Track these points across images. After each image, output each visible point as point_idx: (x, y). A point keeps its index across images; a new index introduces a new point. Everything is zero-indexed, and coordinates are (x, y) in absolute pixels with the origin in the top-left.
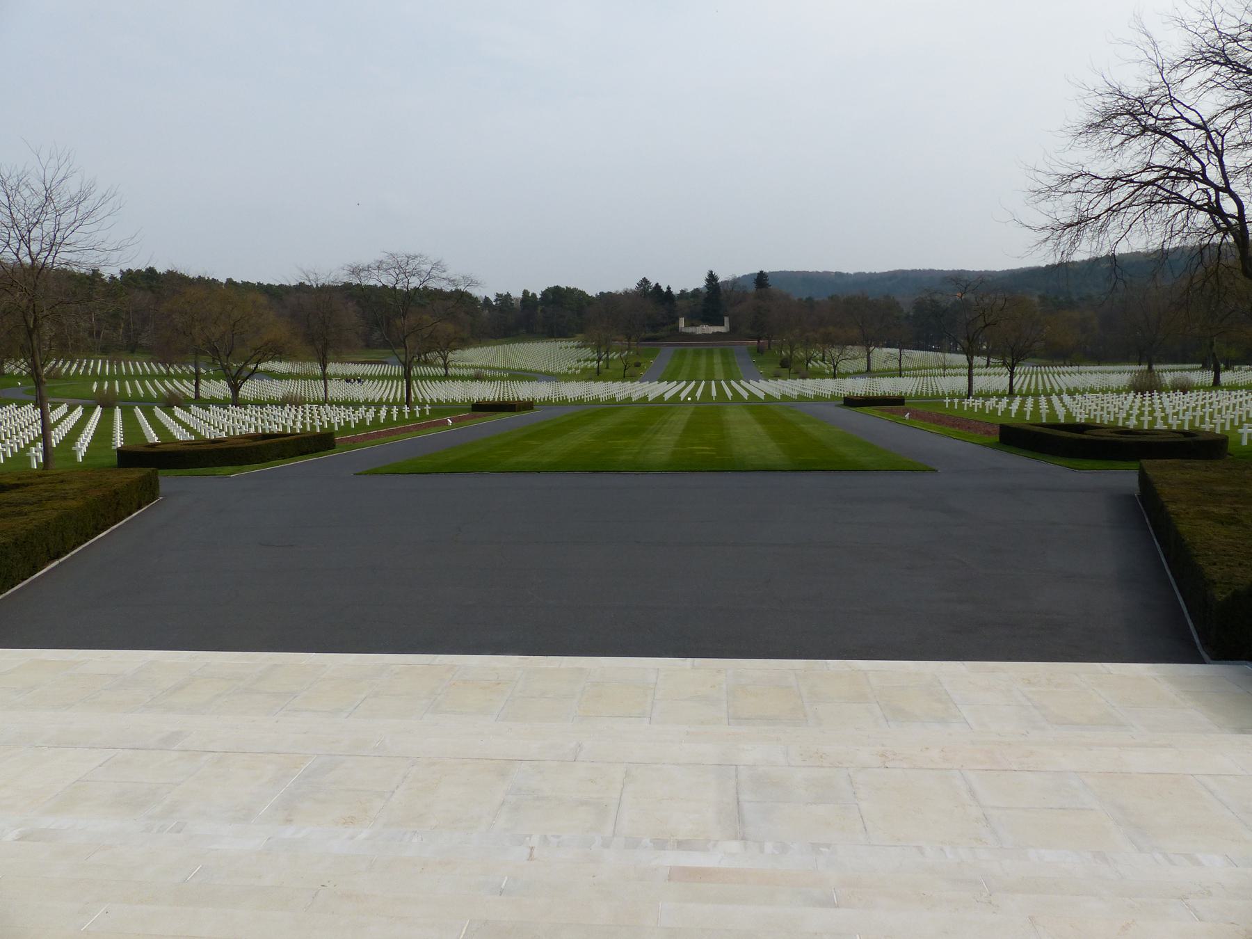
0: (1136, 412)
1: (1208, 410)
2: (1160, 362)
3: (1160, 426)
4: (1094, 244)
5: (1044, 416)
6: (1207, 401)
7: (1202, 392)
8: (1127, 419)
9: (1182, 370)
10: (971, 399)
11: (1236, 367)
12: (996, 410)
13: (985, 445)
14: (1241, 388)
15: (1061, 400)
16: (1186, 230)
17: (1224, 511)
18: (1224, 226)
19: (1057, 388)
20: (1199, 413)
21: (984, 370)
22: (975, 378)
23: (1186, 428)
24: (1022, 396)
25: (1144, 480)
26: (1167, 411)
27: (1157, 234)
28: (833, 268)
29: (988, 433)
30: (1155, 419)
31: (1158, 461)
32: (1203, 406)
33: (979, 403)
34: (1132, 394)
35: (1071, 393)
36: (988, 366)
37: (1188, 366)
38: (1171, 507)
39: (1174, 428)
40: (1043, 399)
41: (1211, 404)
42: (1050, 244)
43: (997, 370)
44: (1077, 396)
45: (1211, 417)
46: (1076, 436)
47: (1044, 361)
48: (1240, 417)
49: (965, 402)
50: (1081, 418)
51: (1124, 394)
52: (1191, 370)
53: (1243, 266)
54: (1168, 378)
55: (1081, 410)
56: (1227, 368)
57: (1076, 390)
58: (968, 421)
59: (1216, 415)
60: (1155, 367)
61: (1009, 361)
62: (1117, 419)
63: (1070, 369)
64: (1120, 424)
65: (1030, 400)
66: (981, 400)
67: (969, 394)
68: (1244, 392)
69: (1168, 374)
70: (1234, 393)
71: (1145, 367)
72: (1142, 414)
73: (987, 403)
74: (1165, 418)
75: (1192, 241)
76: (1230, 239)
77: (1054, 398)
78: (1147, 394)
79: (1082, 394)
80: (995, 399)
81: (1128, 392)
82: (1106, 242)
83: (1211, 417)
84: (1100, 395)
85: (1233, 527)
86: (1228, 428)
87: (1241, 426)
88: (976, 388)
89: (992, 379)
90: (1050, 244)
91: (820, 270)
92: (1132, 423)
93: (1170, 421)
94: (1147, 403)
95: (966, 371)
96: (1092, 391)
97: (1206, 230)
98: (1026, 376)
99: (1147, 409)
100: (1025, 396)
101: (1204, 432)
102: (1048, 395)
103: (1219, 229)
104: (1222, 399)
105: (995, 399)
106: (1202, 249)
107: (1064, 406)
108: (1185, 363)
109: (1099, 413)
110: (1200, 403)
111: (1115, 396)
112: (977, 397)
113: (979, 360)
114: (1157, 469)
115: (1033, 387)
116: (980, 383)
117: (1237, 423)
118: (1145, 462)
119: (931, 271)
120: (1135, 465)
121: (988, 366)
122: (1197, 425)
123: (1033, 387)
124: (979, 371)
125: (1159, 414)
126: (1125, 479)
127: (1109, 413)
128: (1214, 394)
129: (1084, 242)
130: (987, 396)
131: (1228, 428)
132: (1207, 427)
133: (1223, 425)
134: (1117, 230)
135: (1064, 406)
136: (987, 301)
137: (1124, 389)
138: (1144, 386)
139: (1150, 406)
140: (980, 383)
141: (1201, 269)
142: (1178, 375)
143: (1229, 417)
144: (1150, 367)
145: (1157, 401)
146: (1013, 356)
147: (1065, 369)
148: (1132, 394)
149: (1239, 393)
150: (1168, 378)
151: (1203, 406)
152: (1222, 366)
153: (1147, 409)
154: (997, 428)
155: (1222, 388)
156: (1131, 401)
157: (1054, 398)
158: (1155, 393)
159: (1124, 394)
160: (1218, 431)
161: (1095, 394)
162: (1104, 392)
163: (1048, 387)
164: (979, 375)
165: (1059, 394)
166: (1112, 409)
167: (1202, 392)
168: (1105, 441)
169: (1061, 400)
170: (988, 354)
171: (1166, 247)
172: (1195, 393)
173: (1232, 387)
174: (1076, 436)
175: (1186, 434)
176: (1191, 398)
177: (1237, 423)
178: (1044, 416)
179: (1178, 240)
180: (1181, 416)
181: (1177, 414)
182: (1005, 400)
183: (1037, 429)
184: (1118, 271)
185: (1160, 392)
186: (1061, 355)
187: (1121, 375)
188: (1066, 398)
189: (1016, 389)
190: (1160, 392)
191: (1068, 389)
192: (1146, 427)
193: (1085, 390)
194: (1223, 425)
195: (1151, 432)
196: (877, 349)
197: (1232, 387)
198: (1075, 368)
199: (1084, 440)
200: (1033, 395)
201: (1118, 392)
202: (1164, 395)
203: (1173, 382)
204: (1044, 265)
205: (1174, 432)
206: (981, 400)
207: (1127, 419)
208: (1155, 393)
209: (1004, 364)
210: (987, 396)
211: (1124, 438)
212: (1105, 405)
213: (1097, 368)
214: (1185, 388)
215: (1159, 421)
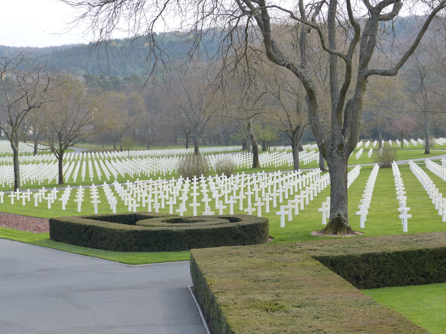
0: (185, 198)
1: (249, 193)
2: (205, 145)
3: (208, 212)
4: (132, 23)
5: (96, 207)
6: (249, 184)
7: (243, 175)
8: (176, 206)
9: (225, 152)
10: (18, 192)
11: (272, 148)
12: (45, 202)
13: (34, 244)
14: (276, 170)
15: (113, 188)
16: (215, 11)
17: (268, 297)
18: (248, 9)
19: (108, 175)
20: (242, 196)
21: (32, 158)
22: (21, 167)
23: (232, 213)
24: (72, 185)
25: (196, 272)
26: (214, 196)
27: (190, 14)
28: (48, 46)
29: (38, 229)
30: (203, 204)
31: (208, 250)
32: (245, 189)
33: (26, 195)
34: (181, 179)
35: (122, 181)
36: (35, 153)
37: (230, 148)
38: (220, 299)
39: (221, 213)
40: (94, 188)
41: (258, 184)
42: (88, 20)
43: (46, 157)
44: (129, 184)
45: (253, 201)
46: (128, 227)
47: (94, 146)
48: (278, 198)
49: (12, 195)
50: (132, 208)
51: (173, 180)
52: (233, 152)
53: (268, 49)
54: (213, 162)
55: (131, 199)
56: (264, 150)
57: (127, 177)
58: (15, 216)
59: (257, 198)
60: (202, 150)
61: (57, 147)
62: (167, 206)
63: (120, 154)
64: (171, 212)
65: (81, 190)
66: (29, 192)
67: (16, 186)
68: (279, 173)
69: (214, 156)
70: (271, 175)
71: (191, 150)
72: (190, 200)
73: (36, 196)
74: (212, 203)
75: (222, 23)
76: (255, 23)
77: (106, 186)
78: (195, 179)
79: (133, 181)
80: (44, 190)
81: (177, 177)
82: (143, 21)
83: (253, 201)
84: (151, 181)
85: (276, 314)
86: (268, 210)
87: (278, 209)
88: (23, 179)
89: (40, 167)
90: (88, 20)
91: (25, 46)
92: (182, 211)
93: (217, 206)
94: (195, 188)
95: (11, 159)
96: (143, 177)
97: (234, 12)
98: (77, 162)
99: (195, 194)
100: (75, 185)
101: (247, 216)
102: (99, 183)
103: (244, 13)
104: (262, 180)
105: (44, 190)
106: (232, 30)
107: (116, 194)
108: (227, 145)
109: (150, 201)
110: (243, 186)
111: (165, 182)
112: (24, 189)
113: (25, 147)
114: (203, 255)
115: (83, 175)
116: (28, 172)
117: (275, 205)
118: (195, 252)
119: (64, 46)
120: (186, 255)
121: (35, 153)
122: (241, 208)
123: (83, 175)
124: (27, 158)
125: (206, 199)
126: (174, 270)
127: (159, 201)
128: (254, 176)
129: (122, 19)
130: (35, 187)
131: (268, 210)
132: (250, 211)
133: (263, 208)
134: (153, 9)
135: (116, 194)
136: (29, 80)
137: (173, 175)
138: (193, 171)
139: (198, 191)
140: (28, 172)
141: (231, 52)
142: (221, 157)
143: (268, 199)
144: (196, 150)
145: (204, 185)
146: (61, 142)
147: (116, 154)
148: (181, 179)
149: (276, 174)
150: (213, 162)
151: (245, 189)
152: (260, 147)
153: (195, 194)
154: (47, 223)
155: (261, 170)
156: (181, 185)
157: (106, 186)
158: (202, 177)
159: (173, 180)
160: (260, 215)
161: (145, 182)
162: (155, 178)
163: (99, 174)
164: (26, 163)
165: (110, 183)
166: (162, 196)
167: (243, 175)
168: (156, 232)
169: (113, 188)
170: (36, 140)
171: (199, 28)
172: (238, 176)
173: (270, 169)
174: (128, 227)
175: (232, 219)
176: (236, 181)
177: (275, 205)
178: (96, 207)
179: (209, 21)
180: (226, 201)
181: (231, 194)
182: (55, 191)
183: (89, 222)
184: (157, 51)
185: (206, 176)
186: (110, 139)
187: (169, 159)
188: (117, 185)
189: (66, 178)
190: (206, 176)
191: (119, 176)
192: (195, 214)
193: (136, 176)
194: (263, 208)
195: (200, 219)
196: (408, 15)
197: (270, 169)
198: (125, 153)
199: (136, 231)
200: (84, 184)
201: (168, 177)
202: (210, 179)
203: (218, 165)
204: (87, 43)
205: (220, 217)
206: (29, 192)
207: (176, 206)
208: (202, 177)
209: (53, 150)
210: (35, 187)
211: (175, 227)
212: (156, 192)
213: (147, 152)
214: (228, 172)
215: (207, 206)
